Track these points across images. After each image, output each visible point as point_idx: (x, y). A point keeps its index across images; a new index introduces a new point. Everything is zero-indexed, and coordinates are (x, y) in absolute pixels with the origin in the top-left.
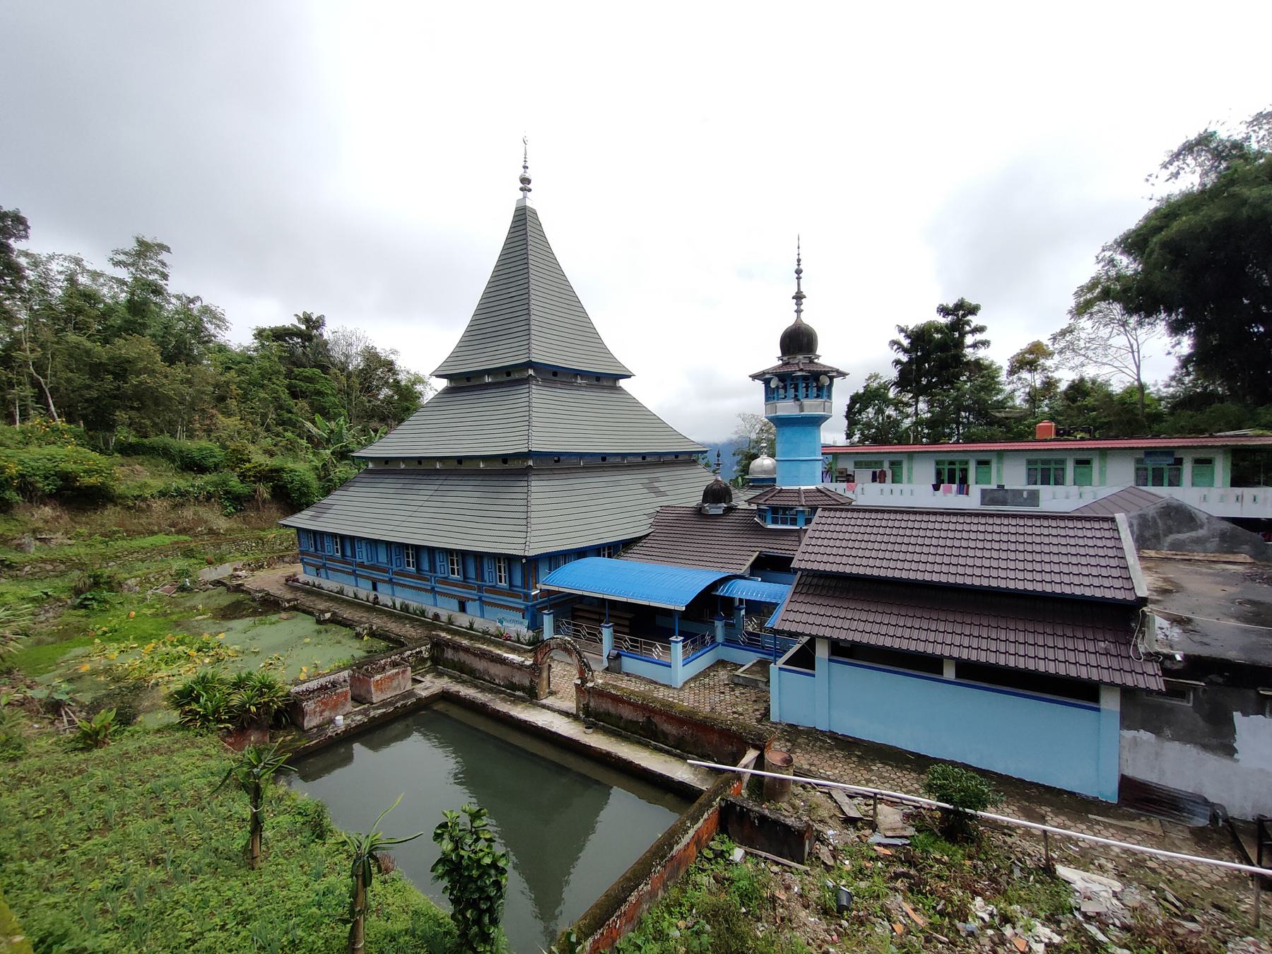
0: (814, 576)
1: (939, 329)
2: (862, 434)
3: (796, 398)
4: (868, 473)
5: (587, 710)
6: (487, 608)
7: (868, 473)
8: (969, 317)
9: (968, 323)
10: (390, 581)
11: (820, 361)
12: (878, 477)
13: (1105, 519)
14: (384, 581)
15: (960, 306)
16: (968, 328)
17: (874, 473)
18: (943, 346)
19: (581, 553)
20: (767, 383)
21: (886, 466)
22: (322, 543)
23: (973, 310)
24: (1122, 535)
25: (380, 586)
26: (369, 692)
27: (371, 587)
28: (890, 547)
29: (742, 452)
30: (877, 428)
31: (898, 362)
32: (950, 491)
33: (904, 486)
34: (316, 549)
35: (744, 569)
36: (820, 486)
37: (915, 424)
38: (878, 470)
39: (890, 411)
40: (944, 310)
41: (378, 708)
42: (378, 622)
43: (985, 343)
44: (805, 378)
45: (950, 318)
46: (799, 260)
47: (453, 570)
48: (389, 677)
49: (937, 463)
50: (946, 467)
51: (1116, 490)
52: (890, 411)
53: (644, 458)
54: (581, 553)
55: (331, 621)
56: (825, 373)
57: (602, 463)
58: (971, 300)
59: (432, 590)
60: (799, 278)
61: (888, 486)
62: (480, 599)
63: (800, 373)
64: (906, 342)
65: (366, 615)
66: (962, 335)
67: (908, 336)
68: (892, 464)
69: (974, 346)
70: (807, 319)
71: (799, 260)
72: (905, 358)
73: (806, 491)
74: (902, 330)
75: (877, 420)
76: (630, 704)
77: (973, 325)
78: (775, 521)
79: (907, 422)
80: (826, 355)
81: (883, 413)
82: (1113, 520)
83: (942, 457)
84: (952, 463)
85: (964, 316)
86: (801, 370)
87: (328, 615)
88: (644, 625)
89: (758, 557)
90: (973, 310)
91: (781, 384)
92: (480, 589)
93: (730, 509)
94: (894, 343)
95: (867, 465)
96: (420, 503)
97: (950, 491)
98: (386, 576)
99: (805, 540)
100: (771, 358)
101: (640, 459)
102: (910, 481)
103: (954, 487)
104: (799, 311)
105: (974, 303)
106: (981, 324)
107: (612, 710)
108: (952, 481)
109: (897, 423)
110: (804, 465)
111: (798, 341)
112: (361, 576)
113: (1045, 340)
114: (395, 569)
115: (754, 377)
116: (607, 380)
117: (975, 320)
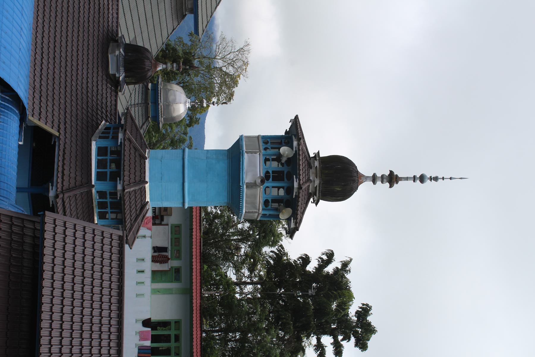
0: (34, 237)
1: (344, 306)
2: (216, 216)
3: (266, 177)
4: (164, 242)
7: (164, 242)
8: (353, 339)
9: (347, 338)
11: (311, 205)
12: (159, 254)
15: (369, 330)
16: (340, 338)
17: (165, 249)
18: (322, 311)
21: (174, 263)
23: (362, 345)
28: (68, 278)
29: (194, 45)
30: (223, 234)
31: (306, 260)
32: (142, 339)
33: (147, 277)
35: (34, 120)
36: (150, 207)
37: (229, 284)
38: (169, 254)
39: (244, 249)
40: (364, 311)
44: (289, 190)
45: (355, 319)
46: (436, 179)
49: (177, 322)
50: (172, 333)
52: (244, 249)
58: (373, 342)
60: (414, 179)
61: (148, 266)
63: (296, 185)
64: (330, 269)
66: (333, 333)
67: (337, 271)
68: (177, 271)
70: (364, 190)
71: (436, 179)
72: (311, 268)
73: (143, 192)
74: (345, 265)
75: (233, 234)
77: (344, 343)
78: (101, 151)
79: (232, 275)
81: (242, 241)
84: (177, 338)
85: (356, 334)
86: (300, 188)
89: (50, 135)
90: (362, 345)
93: (116, 85)
94: (330, 256)
95: (176, 241)
97: (142, 339)
99: (80, 224)
100: (320, 143)
102: (154, 291)
103: (148, 343)
105: (369, 343)
108: (154, 339)
109: (228, 257)
110: (177, 187)
111: (338, 178)
115: (296, 122)
117: (349, 347)
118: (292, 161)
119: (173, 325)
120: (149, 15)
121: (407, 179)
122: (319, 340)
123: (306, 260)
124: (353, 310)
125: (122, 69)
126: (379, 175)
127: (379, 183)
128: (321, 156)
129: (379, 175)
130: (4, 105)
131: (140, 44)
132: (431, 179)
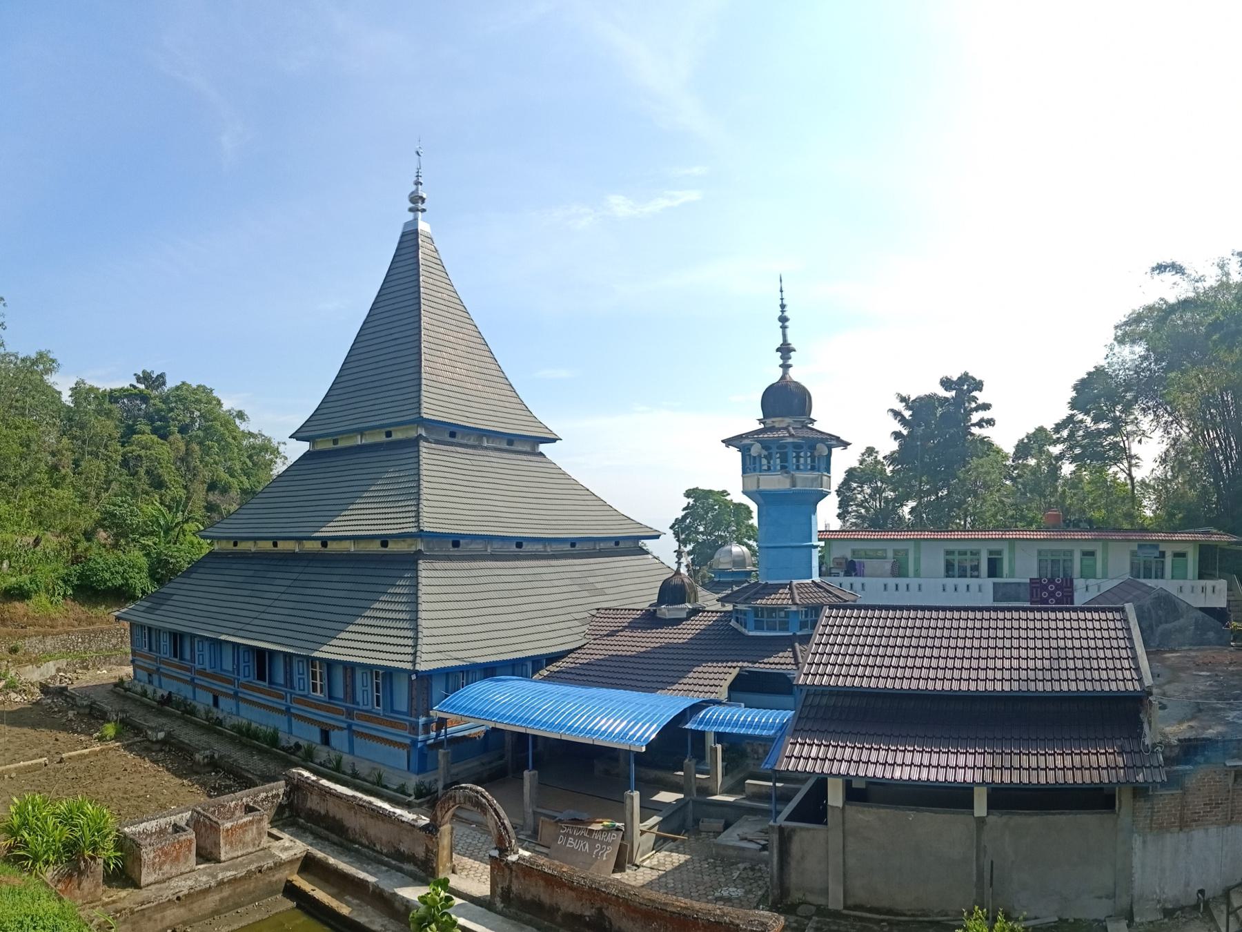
5: (506, 895)
6: (358, 741)
8: (975, 394)
10: (235, 696)
11: (816, 426)
13: (1117, 610)
14: (226, 695)
15: (965, 378)
16: (973, 405)
19: (490, 671)
20: (745, 451)
22: (158, 641)
23: (979, 386)
24: (1132, 626)
25: (222, 700)
26: (217, 845)
27: (211, 702)
31: (897, 435)
34: (150, 649)
40: (946, 383)
41: (227, 869)
42: (221, 749)
43: (990, 422)
44: (797, 447)
46: (783, 306)
47: (314, 685)
48: (241, 826)
51: (1116, 583)
53: (573, 545)
54: (490, 671)
55: (163, 742)
56: (823, 441)
57: (518, 548)
59: (287, 711)
60: (784, 328)
62: (349, 727)
63: (790, 440)
64: (907, 414)
65: (204, 738)
67: (908, 408)
69: (980, 424)
70: (795, 375)
71: (783, 306)
74: (903, 399)
76: (572, 889)
78: (758, 627)
80: (824, 419)
82: (1122, 610)
83: (951, 547)
86: (791, 436)
87: (161, 735)
88: (583, 773)
90: (979, 386)
91: (764, 453)
92: (350, 713)
94: (896, 414)
96: (275, 596)
98: (229, 688)
100: (749, 419)
101: (567, 547)
104: (785, 367)
106: (987, 402)
107: (545, 898)
111: (786, 400)
112: (202, 687)
113: (1049, 426)
114: (243, 680)
115: (728, 442)
116: (528, 443)
117: (982, 397)
118: (766, 445)
119: (949, 557)
120: (637, 581)
121: (784, 335)
122: (974, 425)
123: (897, 435)
124: (942, 393)
125: (683, 606)
126: (781, 362)
127: (790, 362)
128: (761, 417)
129: (781, 362)
130: (357, 788)
131: (657, 590)
132: (783, 312)
